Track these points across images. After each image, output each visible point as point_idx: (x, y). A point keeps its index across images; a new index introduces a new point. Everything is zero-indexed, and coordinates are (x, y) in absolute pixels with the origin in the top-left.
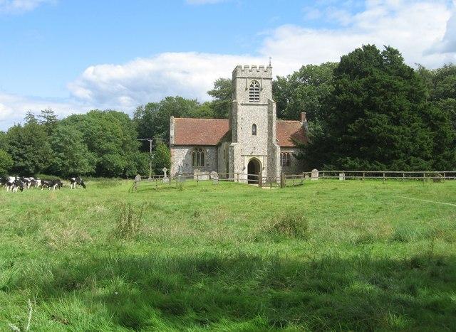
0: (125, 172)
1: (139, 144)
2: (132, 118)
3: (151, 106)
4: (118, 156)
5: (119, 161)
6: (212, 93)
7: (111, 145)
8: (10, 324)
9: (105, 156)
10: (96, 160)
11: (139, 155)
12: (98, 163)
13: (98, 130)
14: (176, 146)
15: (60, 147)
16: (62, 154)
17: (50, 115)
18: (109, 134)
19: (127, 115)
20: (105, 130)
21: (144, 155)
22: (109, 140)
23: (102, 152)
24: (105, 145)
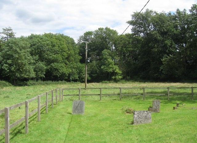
0: (69, 77)
1: (80, 57)
2: (76, 42)
3: (88, 34)
4: (63, 65)
5: (65, 70)
6: (131, 23)
7: (59, 57)
8: (142, 75)
9: (52, 64)
10: (45, 68)
11: (80, 64)
12: (47, 70)
13: (48, 45)
14: (101, 93)
15: (9, 55)
16: (9, 61)
17: (10, 32)
18: (56, 48)
19: (72, 40)
20: (54, 46)
21: (84, 65)
22: (56, 53)
23: (49, 62)
24: (53, 56)
